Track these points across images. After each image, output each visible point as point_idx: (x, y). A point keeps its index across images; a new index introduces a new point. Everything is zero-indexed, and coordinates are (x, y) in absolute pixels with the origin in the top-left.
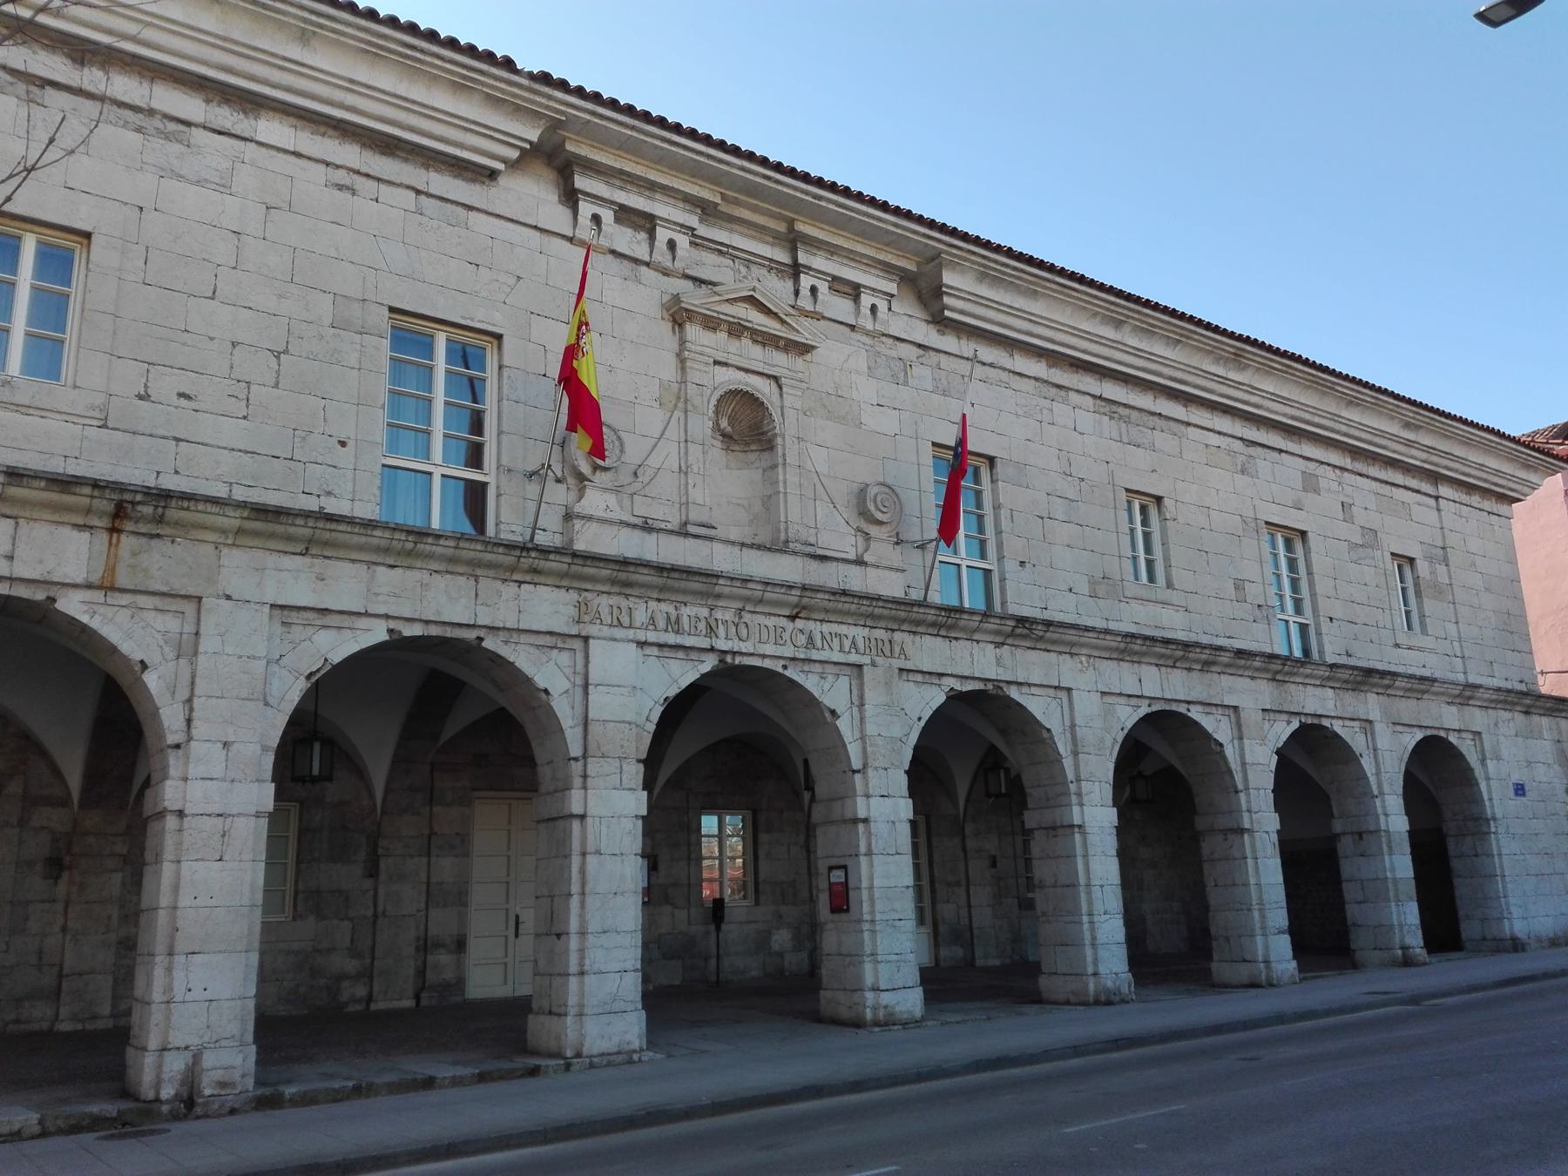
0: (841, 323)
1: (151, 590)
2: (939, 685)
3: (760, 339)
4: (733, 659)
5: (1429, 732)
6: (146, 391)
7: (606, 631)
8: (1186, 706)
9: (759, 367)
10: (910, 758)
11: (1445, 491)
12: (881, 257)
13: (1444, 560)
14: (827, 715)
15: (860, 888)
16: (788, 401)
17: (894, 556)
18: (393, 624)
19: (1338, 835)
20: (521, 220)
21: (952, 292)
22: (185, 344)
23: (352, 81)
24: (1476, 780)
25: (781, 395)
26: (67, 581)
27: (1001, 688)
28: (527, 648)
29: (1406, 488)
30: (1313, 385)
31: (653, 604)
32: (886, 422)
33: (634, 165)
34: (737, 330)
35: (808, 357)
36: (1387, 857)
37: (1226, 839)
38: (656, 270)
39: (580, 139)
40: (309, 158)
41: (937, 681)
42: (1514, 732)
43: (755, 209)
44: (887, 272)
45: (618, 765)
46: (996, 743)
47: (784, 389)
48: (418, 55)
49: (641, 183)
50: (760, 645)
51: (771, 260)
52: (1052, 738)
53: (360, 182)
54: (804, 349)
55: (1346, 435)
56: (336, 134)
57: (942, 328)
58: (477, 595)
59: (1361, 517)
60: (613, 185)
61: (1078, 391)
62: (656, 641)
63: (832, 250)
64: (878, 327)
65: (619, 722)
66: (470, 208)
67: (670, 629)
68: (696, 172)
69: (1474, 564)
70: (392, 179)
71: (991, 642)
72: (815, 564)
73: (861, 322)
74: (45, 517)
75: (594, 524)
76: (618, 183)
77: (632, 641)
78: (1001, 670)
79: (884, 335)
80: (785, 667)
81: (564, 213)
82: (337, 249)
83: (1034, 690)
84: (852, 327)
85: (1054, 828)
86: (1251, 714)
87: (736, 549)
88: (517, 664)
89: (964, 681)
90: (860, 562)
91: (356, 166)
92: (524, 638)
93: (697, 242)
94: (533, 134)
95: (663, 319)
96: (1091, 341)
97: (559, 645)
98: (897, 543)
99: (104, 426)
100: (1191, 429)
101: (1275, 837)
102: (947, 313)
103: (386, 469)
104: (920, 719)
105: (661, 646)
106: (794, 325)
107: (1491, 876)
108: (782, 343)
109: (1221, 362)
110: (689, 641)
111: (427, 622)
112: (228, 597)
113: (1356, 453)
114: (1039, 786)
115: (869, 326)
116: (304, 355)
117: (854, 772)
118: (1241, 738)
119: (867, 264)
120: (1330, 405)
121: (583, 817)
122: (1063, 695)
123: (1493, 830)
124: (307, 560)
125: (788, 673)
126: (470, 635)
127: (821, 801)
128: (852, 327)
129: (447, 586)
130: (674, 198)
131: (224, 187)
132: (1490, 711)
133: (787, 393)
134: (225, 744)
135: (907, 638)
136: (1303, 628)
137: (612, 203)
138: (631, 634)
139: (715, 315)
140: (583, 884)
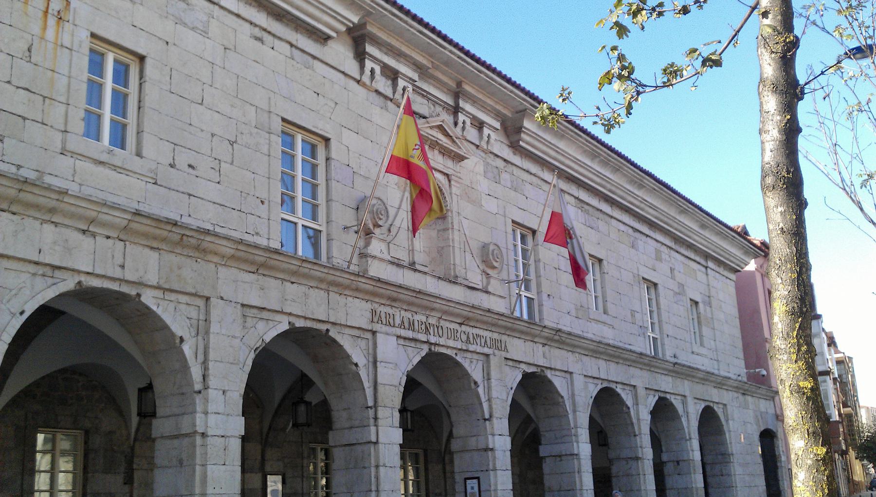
1: (187, 291)
5: (605, 385)
6: (174, 162)
8: (615, 384)
11: (711, 264)
13: (709, 304)
14: (473, 385)
16: (454, 190)
19: (665, 462)
22: (190, 133)
24: (724, 432)
25: (450, 186)
26: (150, 284)
27: (543, 371)
29: (695, 261)
30: (668, 201)
35: (463, 163)
36: (693, 475)
37: (628, 463)
38: (394, 104)
39: (374, 23)
42: (738, 405)
45: (391, 411)
46: (307, 373)
47: (452, 182)
49: (396, 52)
51: (445, 103)
52: (564, 402)
53: (265, 36)
55: (676, 229)
59: (680, 277)
61: (569, 193)
69: (721, 307)
72: (469, 292)
74: (142, 242)
77: (395, 335)
82: (257, 78)
83: (558, 373)
84: (477, 147)
85: (560, 456)
86: (641, 392)
94: (355, 19)
99: (155, 183)
100: (613, 220)
101: (651, 462)
102: (521, 143)
103: (284, 222)
104: (22, 313)
107: (729, 487)
109: (633, 183)
112: (222, 298)
113: (677, 240)
114: (550, 430)
116: (244, 144)
117: (485, 420)
118: (637, 404)
119: (489, 110)
120: (673, 212)
121: (377, 443)
122: (568, 376)
123: (732, 460)
126: (323, 327)
127: (457, 438)
128: (477, 147)
131: (205, 33)
132: (730, 392)
133: (455, 186)
134: (224, 392)
136: (530, 300)
137: (381, 62)
140: (378, 486)
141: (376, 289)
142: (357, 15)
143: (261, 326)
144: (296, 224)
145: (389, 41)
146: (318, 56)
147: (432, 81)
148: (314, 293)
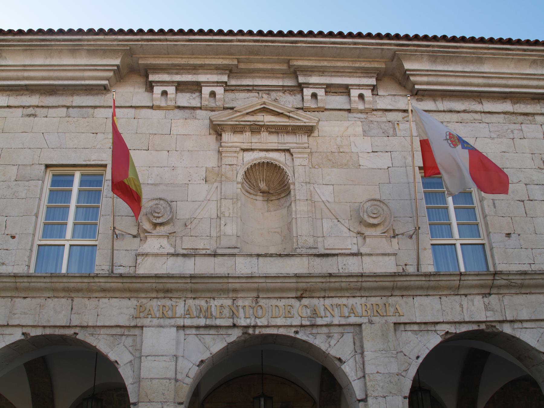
0: (340, 110)
2: (435, 331)
3: (273, 130)
4: (254, 331)
7: (155, 322)
9: (275, 146)
10: (410, 387)
12: (357, 65)
17: (384, 245)
18: (25, 330)
20: (123, 105)
21: (415, 73)
23: (24, 66)
28: (105, 336)
31: (190, 302)
32: (383, 161)
33: (180, 59)
34: (256, 129)
35: (316, 133)
38: (206, 110)
40: (15, 107)
41: (433, 328)
43: (264, 62)
47: (295, 156)
48: (48, 43)
49: (189, 68)
50: (273, 319)
51: (283, 86)
54: (309, 130)
56: (28, 93)
57: (420, 97)
58: (72, 309)
60: (172, 73)
62: (191, 325)
63: (322, 71)
64: (367, 106)
65: (162, 379)
66: (95, 107)
67: (201, 316)
68: (217, 53)
70: (54, 105)
71: (478, 294)
73: (354, 106)
75: (150, 257)
76: (175, 71)
77: (173, 326)
78: (489, 314)
79: (373, 110)
80: (297, 332)
81: (147, 95)
82: (23, 144)
83: (525, 325)
84: (349, 111)
87: (254, 260)
89: (457, 325)
90: (358, 254)
91: (36, 104)
92: (103, 331)
93: (228, 88)
95: (210, 134)
98: (394, 237)
102: (417, 87)
104: (418, 357)
105: (198, 327)
106: (295, 117)
110: (218, 322)
111: (44, 327)
115: (361, 106)
125: (298, 336)
126: (69, 332)
128: (349, 111)
129: (54, 305)
133: (296, 158)
137: (173, 82)
138: (172, 321)
139: (237, 123)
142: (117, 58)
144: (455, 244)
145: (170, 62)
146: (98, 104)
147: (258, 75)
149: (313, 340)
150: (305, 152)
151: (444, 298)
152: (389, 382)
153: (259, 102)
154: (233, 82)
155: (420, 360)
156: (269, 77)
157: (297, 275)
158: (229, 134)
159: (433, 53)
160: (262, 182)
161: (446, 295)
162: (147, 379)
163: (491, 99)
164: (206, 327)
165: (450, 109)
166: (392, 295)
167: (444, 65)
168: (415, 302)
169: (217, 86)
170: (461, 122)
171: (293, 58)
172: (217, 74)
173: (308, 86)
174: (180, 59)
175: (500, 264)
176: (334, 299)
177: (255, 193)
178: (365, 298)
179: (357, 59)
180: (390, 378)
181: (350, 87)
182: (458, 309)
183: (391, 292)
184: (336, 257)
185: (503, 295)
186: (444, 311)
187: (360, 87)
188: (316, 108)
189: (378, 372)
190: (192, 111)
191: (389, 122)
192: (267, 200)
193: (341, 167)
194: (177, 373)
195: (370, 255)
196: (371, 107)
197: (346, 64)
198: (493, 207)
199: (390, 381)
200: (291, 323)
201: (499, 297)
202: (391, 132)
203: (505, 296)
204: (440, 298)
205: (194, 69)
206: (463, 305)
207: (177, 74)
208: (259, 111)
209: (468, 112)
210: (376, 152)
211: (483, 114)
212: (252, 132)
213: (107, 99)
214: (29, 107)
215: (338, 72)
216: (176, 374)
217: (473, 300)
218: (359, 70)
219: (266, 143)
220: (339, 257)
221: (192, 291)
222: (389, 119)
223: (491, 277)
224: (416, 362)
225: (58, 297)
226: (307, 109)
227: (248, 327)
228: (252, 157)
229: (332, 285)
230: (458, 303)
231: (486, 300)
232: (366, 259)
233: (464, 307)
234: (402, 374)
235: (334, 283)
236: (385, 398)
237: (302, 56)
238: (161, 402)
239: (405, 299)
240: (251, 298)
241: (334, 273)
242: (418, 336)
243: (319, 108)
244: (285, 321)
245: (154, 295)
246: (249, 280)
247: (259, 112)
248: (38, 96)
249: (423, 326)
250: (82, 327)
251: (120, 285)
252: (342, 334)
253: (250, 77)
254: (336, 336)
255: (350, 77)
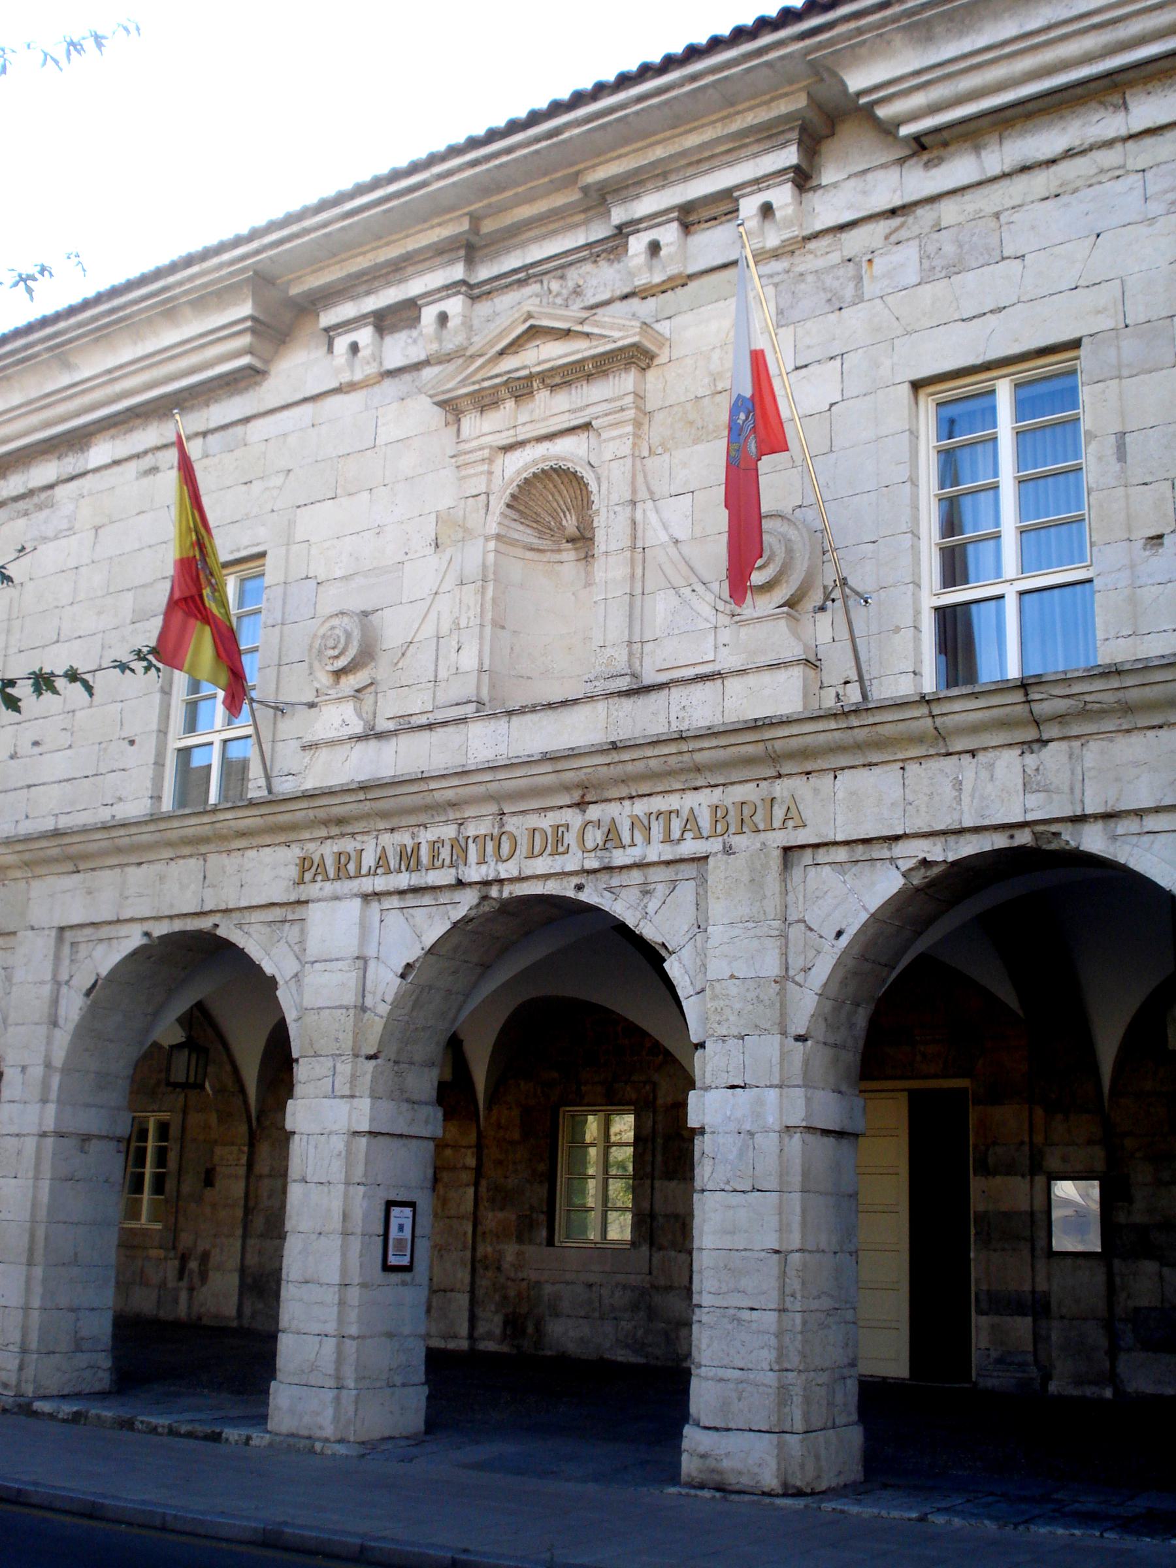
3: (558, 380)
4: (501, 891)
12: (736, 125)
15: (363, 1235)
20: (290, 401)
21: (882, 94)
23: (109, 371)
28: (258, 926)
31: (386, 839)
41: (886, 854)
44: (770, 137)
49: (384, 271)
58: (205, 877)
66: (247, 420)
76: (364, 288)
77: (356, 895)
78: (1033, 800)
80: (579, 887)
83: (1151, 823)
88: (246, 950)
89: (952, 839)
93: (475, 292)
96: (949, 76)
97: (289, 918)
104: (839, 934)
108: (589, 366)
112: (33, 928)
124: (77, 877)
125: (583, 897)
126: (205, 924)
130: (425, 260)
135: (797, 785)
137: (364, 316)
141: (271, 819)
143: (100, 949)
145: (343, 273)
146: (249, 413)
147: (531, 234)
148: (175, 868)
149: (611, 902)
150: (623, 419)
151: (912, 768)
152: (755, 1001)
153: (516, 316)
154: (484, 272)
155: (844, 940)
156: (554, 233)
157: (548, 756)
158: (473, 415)
159: (909, 17)
160: (567, 513)
161: (919, 759)
162: (313, 1009)
163: (1159, 80)
164: (415, 890)
165: (1023, 164)
166: (780, 776)
167: (960, 37)
168: (836, 787)
169: (449, 296)
170: (1057, 196)
171: (581, 166)
172: (444, 265)
173: (637, 227)
174: (360, 259)
175: (1107, 639)
176: (653, 799)
177: (555, 547)
178: (721, 788)
179: (731, 110)
180: (758, 990)
181: (736, 194)
182: (948, 792)
183: (775, 767)
184: (394, 740)
185: (1083, 741)
186: (910, 804)
187: (761, 186)
188: (664, 282)
189: (732, 977)
190: (415, 374)
191: (849, 260)
192: (586, 557)
193: (715, 435)
194: (367, 994)
195: (742, 672)
196: (796, 233)
197: (708, 134)
198: (1113, 459)
199: (758, 997)
200: (562, 868)
201: (1070, 748)
202: (849, 292)
203: (1091, 743)
204: (902, 768)
205: (397, 269)
206: (964, 783)
207: (368, 293)
208: (525, 338)
209: (1083, 152)
210: (806, 366)
211: (1130, 144)
212: (516, 397)
213: (272, 391)
214: (146, 453)
215: (699, 162)
216: (364, 997)
217: (993, 764)
218: (748, 137)
219: (544, 420)
220: (673, 690)
221: (384, 815)
222: (848, 254)
223: (1018, 696)
224: (833, 946)
225: (184, 857)
226: (645, 290)
227: (486, 883)
228: (521, 464)
229: (630, 767)
230: (951, 779)
231: (1031, 760)
232: (734, 685)
233: (964, 787)
234: (797, 978)
235: (628, 761)
236: (743, 1039)
237: (599, 155)
238: (332, 1055)
239: (813, 779)
240: (491, 817)
241: (621, 741)
242: (847, 877)
243: (670, 279)
244: (550, 863)
245: (323, 832)
246: (466, 780)
247: (529, 340)
248: (155, 424)
249: (860, 848)
250: (227, 911)
251: (259, 821)
252: (673, 884)
253: (516, 247)
254: (661, 889)
255: (729, 164)
